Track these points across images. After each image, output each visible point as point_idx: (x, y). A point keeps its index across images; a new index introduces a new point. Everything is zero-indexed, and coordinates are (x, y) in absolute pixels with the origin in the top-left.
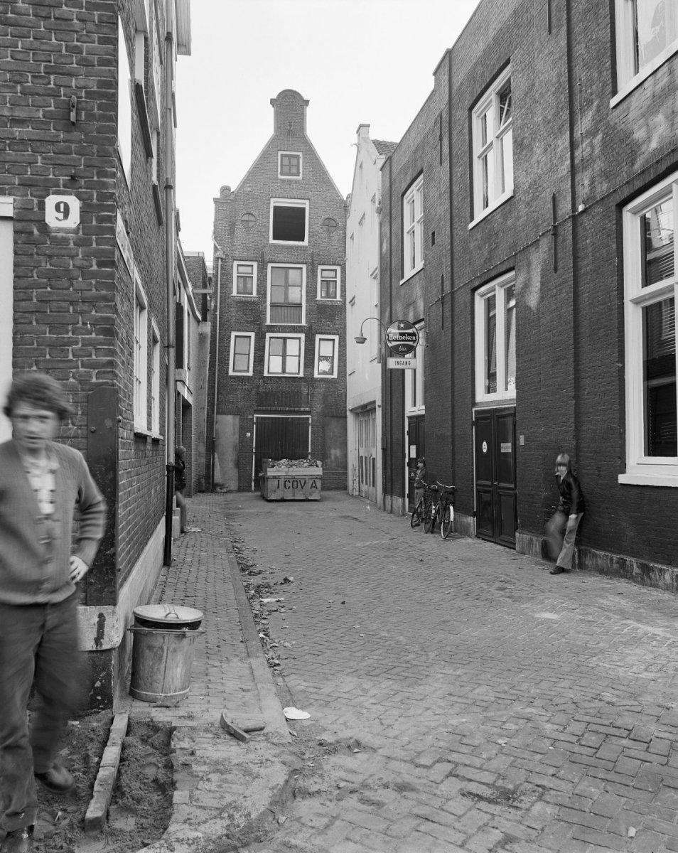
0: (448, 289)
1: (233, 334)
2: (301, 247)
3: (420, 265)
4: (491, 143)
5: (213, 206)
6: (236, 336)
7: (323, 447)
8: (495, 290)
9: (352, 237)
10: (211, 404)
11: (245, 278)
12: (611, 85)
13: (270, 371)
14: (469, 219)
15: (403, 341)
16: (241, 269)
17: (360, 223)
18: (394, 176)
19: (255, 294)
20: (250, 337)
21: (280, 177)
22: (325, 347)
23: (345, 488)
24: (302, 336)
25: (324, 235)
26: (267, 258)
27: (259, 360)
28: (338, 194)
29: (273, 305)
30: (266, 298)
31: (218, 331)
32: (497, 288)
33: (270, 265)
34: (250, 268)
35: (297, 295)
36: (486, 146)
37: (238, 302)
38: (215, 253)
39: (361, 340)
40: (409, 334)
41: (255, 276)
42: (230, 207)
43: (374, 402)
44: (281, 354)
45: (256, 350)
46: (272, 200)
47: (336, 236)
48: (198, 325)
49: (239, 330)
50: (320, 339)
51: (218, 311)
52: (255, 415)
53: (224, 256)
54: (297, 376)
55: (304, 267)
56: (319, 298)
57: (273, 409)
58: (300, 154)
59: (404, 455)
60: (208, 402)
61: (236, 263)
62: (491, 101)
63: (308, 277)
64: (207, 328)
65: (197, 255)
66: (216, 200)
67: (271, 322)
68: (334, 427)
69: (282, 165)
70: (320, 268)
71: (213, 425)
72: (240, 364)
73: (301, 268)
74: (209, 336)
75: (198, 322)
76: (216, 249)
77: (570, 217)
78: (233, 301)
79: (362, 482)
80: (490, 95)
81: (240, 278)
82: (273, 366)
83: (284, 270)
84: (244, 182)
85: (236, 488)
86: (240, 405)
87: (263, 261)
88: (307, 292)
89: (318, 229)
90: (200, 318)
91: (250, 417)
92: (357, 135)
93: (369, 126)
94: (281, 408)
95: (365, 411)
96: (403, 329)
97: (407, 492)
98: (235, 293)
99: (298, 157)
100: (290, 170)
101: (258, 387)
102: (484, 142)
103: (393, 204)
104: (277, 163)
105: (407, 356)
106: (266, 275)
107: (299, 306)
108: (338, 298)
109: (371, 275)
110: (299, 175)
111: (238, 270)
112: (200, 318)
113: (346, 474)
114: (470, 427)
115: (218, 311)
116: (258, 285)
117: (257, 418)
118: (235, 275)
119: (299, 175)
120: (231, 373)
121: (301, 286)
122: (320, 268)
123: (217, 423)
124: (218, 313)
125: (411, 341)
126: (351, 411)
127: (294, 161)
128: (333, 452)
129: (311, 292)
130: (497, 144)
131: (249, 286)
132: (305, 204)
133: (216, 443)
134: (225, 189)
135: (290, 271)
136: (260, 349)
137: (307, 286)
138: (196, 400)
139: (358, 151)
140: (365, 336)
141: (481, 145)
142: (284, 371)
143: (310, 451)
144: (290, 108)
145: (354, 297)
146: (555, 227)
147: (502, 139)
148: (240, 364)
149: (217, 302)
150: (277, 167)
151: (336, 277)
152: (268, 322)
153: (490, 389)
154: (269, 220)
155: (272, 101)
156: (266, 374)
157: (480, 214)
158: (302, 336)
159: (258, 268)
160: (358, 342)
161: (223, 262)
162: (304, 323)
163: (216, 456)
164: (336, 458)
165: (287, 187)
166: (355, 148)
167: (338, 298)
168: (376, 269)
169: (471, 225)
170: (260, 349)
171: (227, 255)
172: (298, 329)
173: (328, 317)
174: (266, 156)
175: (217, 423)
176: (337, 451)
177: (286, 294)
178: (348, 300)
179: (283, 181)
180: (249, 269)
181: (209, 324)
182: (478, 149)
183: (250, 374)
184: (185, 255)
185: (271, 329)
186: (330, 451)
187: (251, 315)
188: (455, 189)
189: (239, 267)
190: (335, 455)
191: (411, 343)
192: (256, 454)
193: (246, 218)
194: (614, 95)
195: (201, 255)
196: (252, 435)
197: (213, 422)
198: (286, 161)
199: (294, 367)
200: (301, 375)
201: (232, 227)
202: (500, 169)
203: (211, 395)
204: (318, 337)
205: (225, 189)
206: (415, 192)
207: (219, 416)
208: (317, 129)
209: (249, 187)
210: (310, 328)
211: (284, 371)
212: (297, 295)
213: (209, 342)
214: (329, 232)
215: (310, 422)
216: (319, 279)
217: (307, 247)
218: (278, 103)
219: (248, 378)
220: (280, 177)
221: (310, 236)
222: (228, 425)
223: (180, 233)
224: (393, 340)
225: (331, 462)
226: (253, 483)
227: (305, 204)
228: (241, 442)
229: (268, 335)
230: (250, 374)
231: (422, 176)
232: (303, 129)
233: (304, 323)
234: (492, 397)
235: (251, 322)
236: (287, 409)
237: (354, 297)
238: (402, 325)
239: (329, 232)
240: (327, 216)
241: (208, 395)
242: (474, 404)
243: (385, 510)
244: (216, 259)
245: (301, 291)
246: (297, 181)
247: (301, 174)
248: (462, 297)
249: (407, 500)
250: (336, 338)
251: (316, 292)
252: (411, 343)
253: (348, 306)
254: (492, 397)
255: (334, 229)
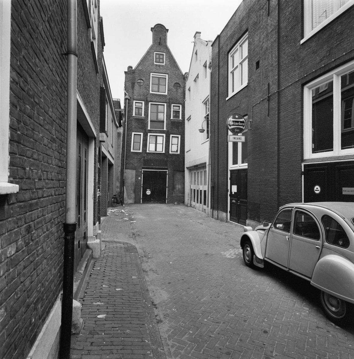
0: (274, 89)
1: (133, 133)
2: (164, 95)
3: (245, 84)
4: (237, 67)
5: (124, 75)
6: (134, 134)
7: (173, 184)
8: (333, 78)
9: (189, 90)
10: (122, 164)
11: (139, 109)
12: (301, 30)
13: (150, 150)
14: (300, 38)
15: (237, 125)
16: (137, 104)
17: (195, 81)
18: (221, 45)
19: (143, 115)
20: (140, 135)
21: (155, 63)
22: (175, 142)
23: (183, 202)
24: (164, 135)
25: (175, 90)
26: (149, 99)
27: (145, 145)
28: (181, 72)
29: (151, 121)
30: (148, 117)
31: (126, 138)
32: (335, 76)
33: (150, 103)
34: (141, 104)
35: (162, 116)
36: (234, 68)
37: (136, 119)
38: (125, 97)
39: (202, 131)
40: (241, 122)
41: (143, 107)
42: (133, 77)
43: (205, 163)
44: (155, 143)
45: (143, 141)
46: (151, 74)
47: (180, 91)
48: (117, 129)
49: (136, 132)
50: (172, 137)
51: (126, 122)
52: (143, 170)
53: (129, 98)
54: (162, 152)
55: (165, 104)
56: (172, 118)
57: (151, 167)
58: (164, 54)
59: (228, 190)
60: (121, 164)
61: (134, 102)
62: (238, 49)
63: (167, 109)
64: (121, 130)
65: (117, 100)
66: (125, 72)
67: (150, 128)
68: (178, 176)
69: (156, 58)
70: (172, 105)
71: (123, 174)
72: (136, 147)
73: (164, 105)
74: (122, 134)
75: (117, 127)
76: (125, 94)
77: (277, 92)
78: (133, 118)
79: (192, 200)
80: (238, 46)
81: (136, 109)
82: (151, 148)
83: (156, 106)
84: (139, 65)
85: (134, 202)
86: (136, 165)
87: (147, 101)
88: (166, 115)
89: (172, 87)
90: (118, 125)
91: (140, 170)
92: (194, 38)
93: (200, 33)
94: (154, 167)
95: (198, 168)
96: (237, 119)
97: (229, 210)
98: (134, 115)
99: (163, 55)
100: (159, 60)
101: (144, 157)
102: (233, 67)
103: (221, 60)
104: (154, 57)
105: (239, 134)
106: (148, 107)
107: (163, 122)
108: (180, 118)
109: (203, 102)
110: (163, 63)
111: (135, 105)
112: (118, 125)
113: (184, 196)
114: (300, 175)
115: (126, 122)
116: (144, 112)
117: (143, 171)
118: (134, 107)
119: (163, 63)
120: (132, 151)
121: (164, 113)
122: (172, 105)
123: (125, 173)
124: (126, 124)
125: (242, 126)
126: (187, 168)
127: (161, 57)
128: (177, 186)
129: (168, 116)
130: (240, 67)
131: (140, 112)
132: (166, 76)
133: (125, 182)
134: (130, 67)
135: (159, 106)
136: (145, 140)
137: (167, 113)
138: (115, 162)
139: (195, 46)
140: (204, 129)
141: (232, 67)
142: (156, 150)
143: (167, 186)
144: (159, 32)
145: (190, 116)
146: (269, 97)
147: (242, 64)
148: (136, 147)
149: (126, 119)
150: (154, 59)
151: (179, 109)
152: (149, 128)
153: (235, 162)
154: (150, 83)
155: (152, 29)
156: (148, 151)
157: (231, 94)
158: (164, 135)
159: (145, 104)
160: (200, 132)
161: (129, 101)
162: (165, 129)
163: (125, 188)
164: (179, 189)
165: (158, 68)
166: (193, 43)
167: (180, 118)
168: (208, 96)
169: (302, 42)
170: (145, 140)
171: (131, 98)
172: (163, 132)
173: (177, 127)
174: (148, 53)
175: (125, 173)
176: (179, 186)
177: (157, 116)
178: (186, 118)
179: (156, 65)
180: (140, 105)
181: (122, 128)
182: (230, 69)
183: (141, 151)
184: (113, 100)
185: (150, 131)
186: (176, 186)
187: (141, 124)
188: (283, 25)
189: (136, 103)
190: (178, 188)
191: (242, 127)
192: (143, 187)
193: (139, 81)
194: (227, 97)
195: (119, 100)
196: (141, 178)
197: (123, 172)
198: (157, 56)
199: (161, 149)
200: (164, 152)
201: (133, 85)
202: (241, 77)
203: (123, 160)
204: (171, 136)
205: (130, 67)
206: (238, 47)
207: (126, 170)
208: (172, 42)
209: (141, 67)
210: (168, 131)
211: (156, 150)
212: (162, 116)
213: (122, 136)
214: (177, 89)
215: (167, 173)
216: (172, 110)
217: (166, 95)
218: (155, 30)
219: (140, 153)
220: (155, 63)
221: (168, 91)
222: (130, 175)
223: (104, 47)
224: (232, 125)
225: (177, 191)
226: (141, 200)
227: (166, 76)
228: (136, 181)
229: (149, 134)
230: (141, 151)
231: (247, 33)
232: (165, 42)
233: (165, 129)
234: (323, 156)
235: (141, 128)
236: (157, 167)
237: (190, 116)
238: (237, 117)
239: (177, 89)
240: (176, 82)
241: (121, 160)
242: (303, 160)
243: (213, 217)
244: (126, 99)
245: (164, 115)
246: (162, 66)
247: (164, 63)
248: (288, 95)
249: (229, 214)
250: (180, 136)
251: (171, 116)
252: (242, 127)
253: (186, 122)
254: (323, 156)
255: (178, 88)
